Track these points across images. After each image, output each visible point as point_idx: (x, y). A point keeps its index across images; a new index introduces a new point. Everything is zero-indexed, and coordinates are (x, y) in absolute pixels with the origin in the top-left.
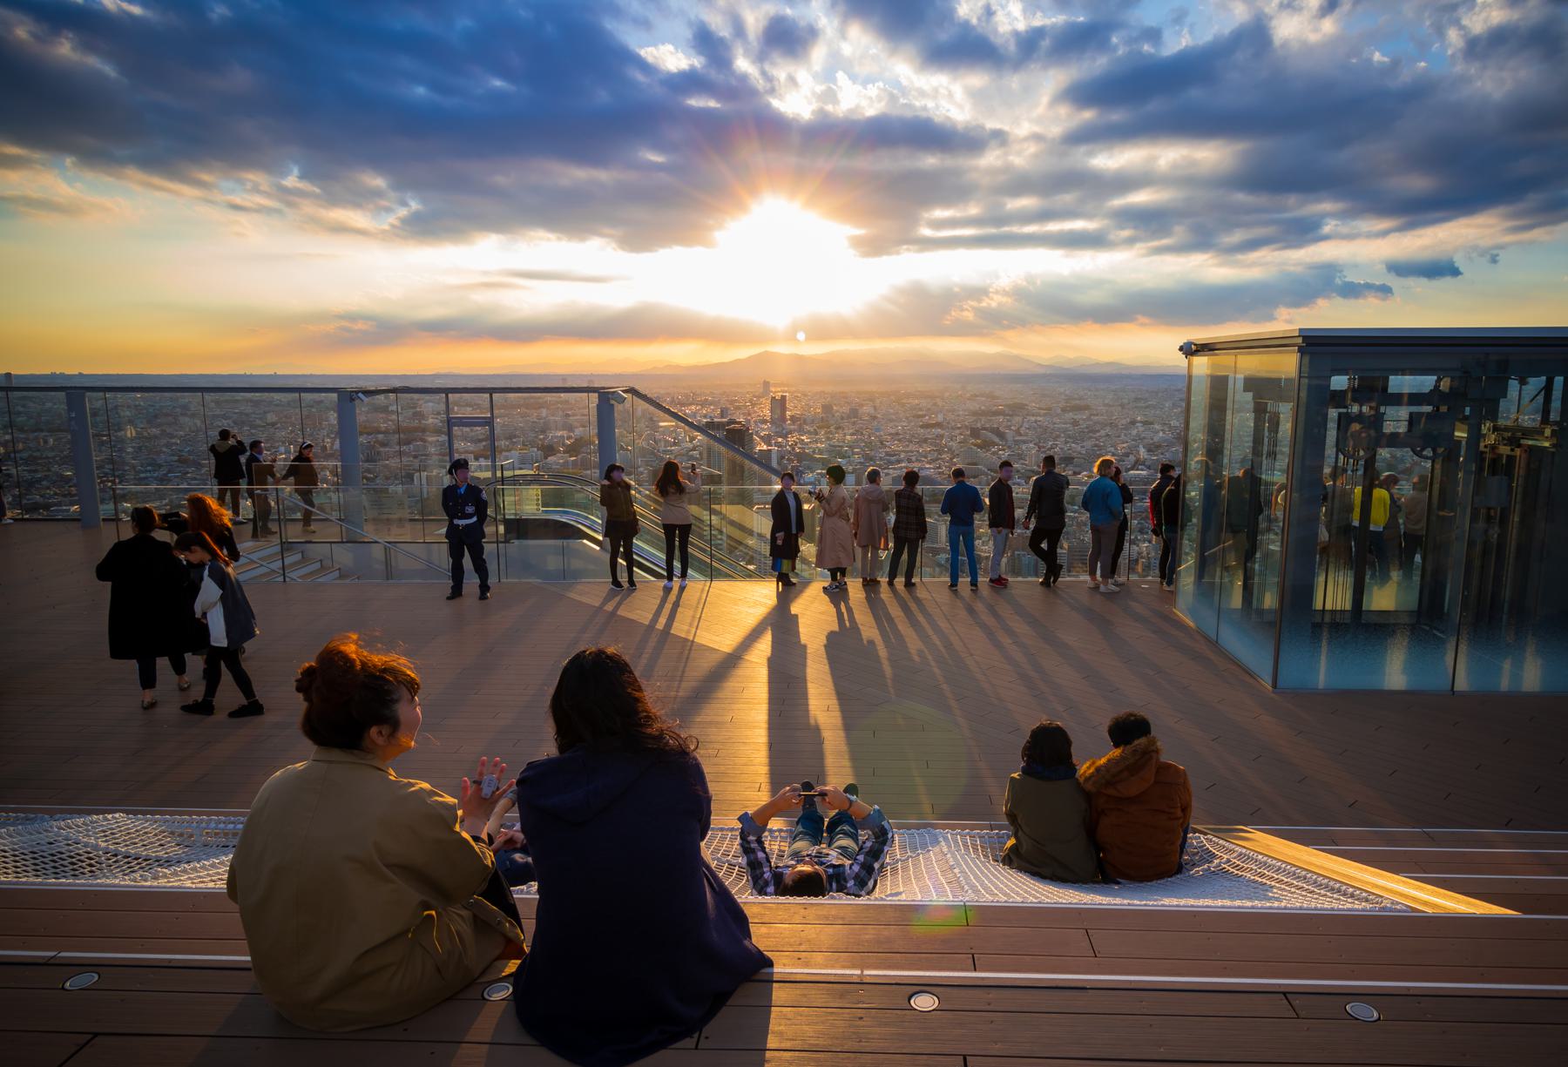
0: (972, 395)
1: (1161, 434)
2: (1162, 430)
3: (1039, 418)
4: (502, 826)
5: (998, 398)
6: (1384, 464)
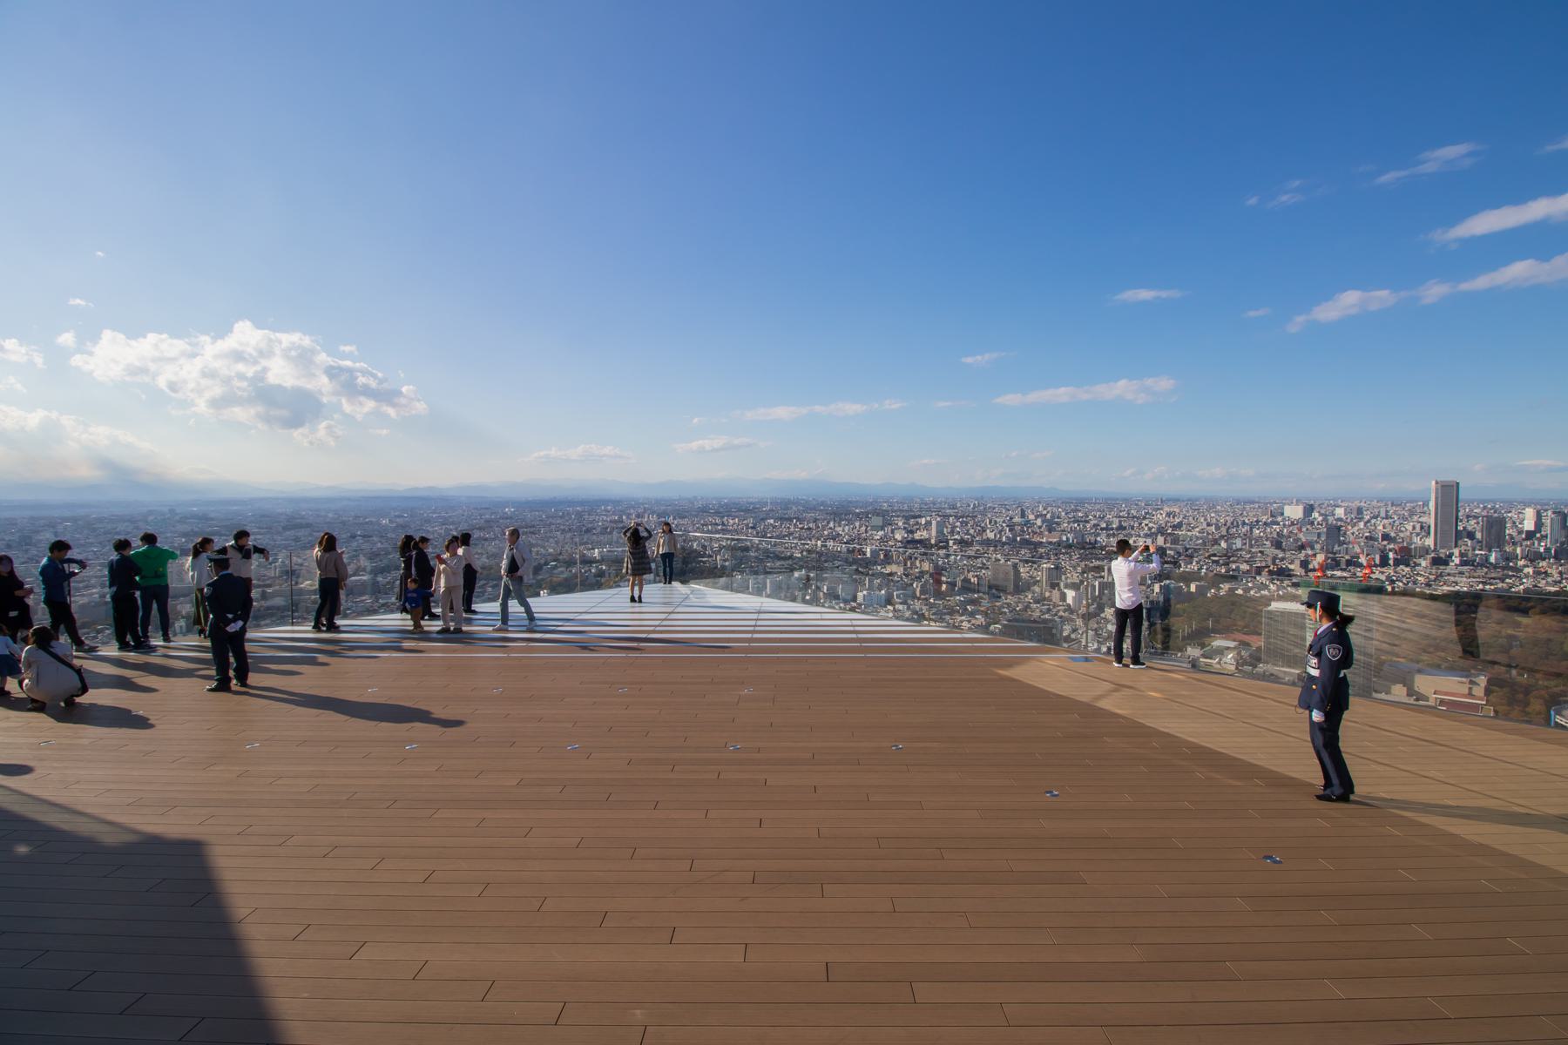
0: (181, 518)
1: (379, 545)
2: (380, 542)
3: (259, 537)
4: (1163, 564)
5: (212, 519)
6: (977, 616)
